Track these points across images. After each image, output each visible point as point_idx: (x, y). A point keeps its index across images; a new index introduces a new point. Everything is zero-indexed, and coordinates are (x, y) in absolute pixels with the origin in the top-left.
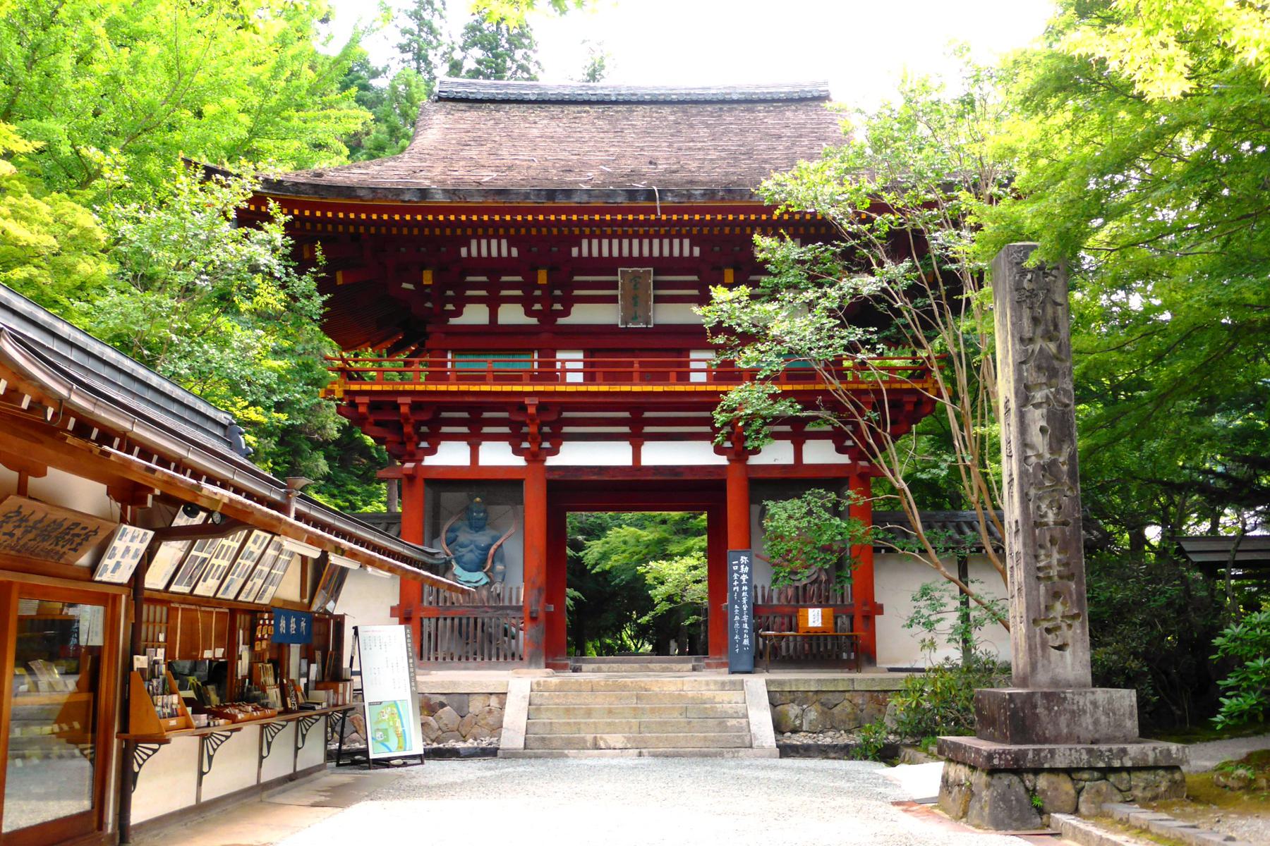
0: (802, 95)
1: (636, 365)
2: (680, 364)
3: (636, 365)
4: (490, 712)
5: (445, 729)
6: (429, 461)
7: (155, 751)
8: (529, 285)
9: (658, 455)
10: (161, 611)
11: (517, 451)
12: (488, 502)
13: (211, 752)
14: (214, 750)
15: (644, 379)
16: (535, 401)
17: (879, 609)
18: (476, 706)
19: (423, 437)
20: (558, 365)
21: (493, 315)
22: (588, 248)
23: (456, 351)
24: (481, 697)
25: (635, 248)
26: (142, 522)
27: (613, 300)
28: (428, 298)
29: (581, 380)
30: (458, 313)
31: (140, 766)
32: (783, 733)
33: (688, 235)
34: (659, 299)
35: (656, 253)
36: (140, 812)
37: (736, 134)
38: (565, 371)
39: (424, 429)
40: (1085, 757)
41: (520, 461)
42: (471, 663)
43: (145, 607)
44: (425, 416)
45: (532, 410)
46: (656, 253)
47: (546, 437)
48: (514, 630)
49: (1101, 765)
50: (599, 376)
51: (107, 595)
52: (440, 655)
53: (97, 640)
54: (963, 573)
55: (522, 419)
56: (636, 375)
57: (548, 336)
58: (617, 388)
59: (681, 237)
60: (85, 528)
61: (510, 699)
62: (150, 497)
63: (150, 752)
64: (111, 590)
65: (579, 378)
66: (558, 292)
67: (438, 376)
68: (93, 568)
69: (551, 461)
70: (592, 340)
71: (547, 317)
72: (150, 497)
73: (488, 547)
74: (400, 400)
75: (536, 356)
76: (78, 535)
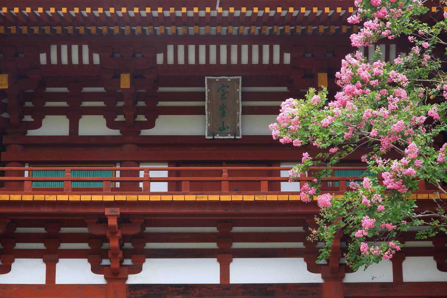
1: (225, 174)
3: (225, 174)
8: (112, 96)
9: (246, 272)
11: (96, 269)
15: (235, 188)
16: (117, 211)
20: (142, 174)
21: (74, 127)
22: (174, 55)
23: (31, 163)
27: (200, 111)
34: (247, 111)
41: (99, 279)
45: (113, 222)
46: (245, 60)
56: (225, 185)
57: (133, 148)
58: (204, 198)
65: (163, 187)
69: (133, 279)
70: (177, 153)
71: (131, 129)
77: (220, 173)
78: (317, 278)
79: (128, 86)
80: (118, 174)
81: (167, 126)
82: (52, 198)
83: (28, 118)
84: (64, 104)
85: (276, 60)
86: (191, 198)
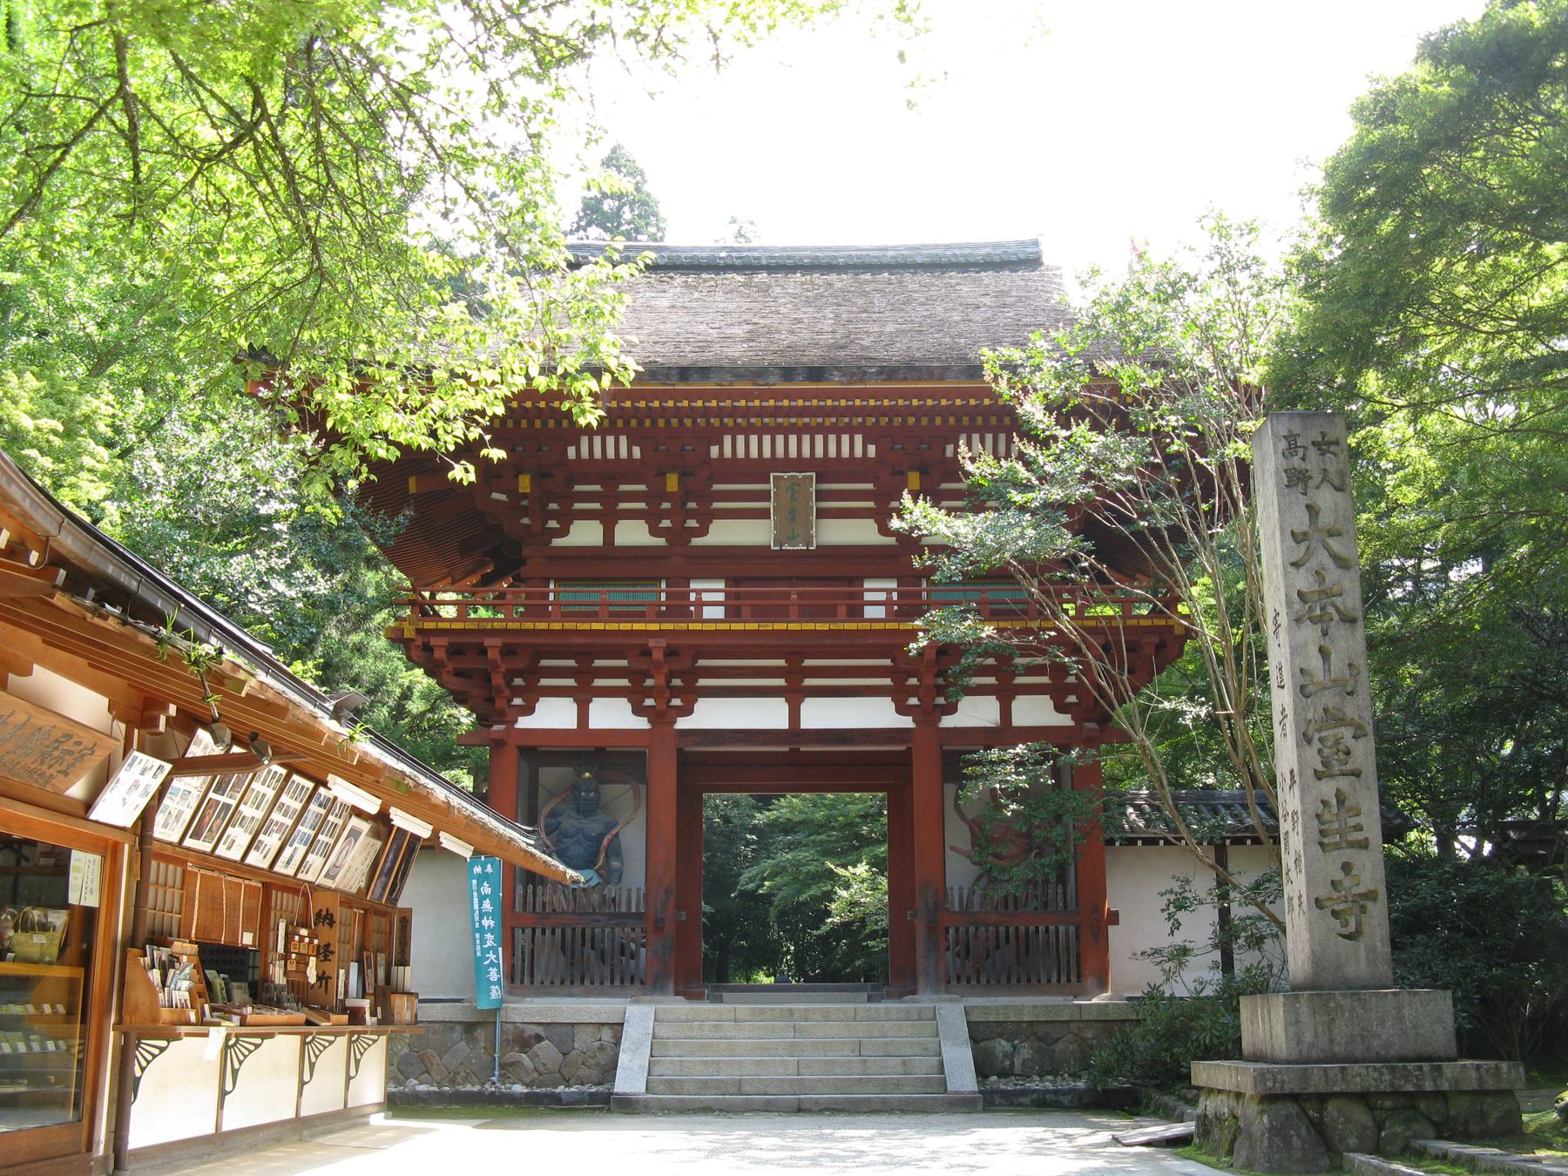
0: (1006, 258)
2: (851, 596)
4: (601, 1048)
5: (542, 1069)
6: (524, 723)
7: (162, 1050)
8: (655, 496)
9: (820, 714)
10: (174, 872)
11: (638, 710)
12: (601, 779)
13: (236, 1065)
14: (241, 1063)
15: (804, 615)
16: (663, 642)
17: (1114, 918)
18: (583, 1040)
19: (517, 691)
20: (693, 597)
21: (609, 534)
22: (732, 447)
23: (557, 580)
24: (590, 1029)
25: (793, 446)
26: (157, 750)
27: (764, 514)
28: (525, 512)
29: (722, 616)
30: (564, 532)
31: (143, 1069)
32: (987, 1077)
33: (861, 429)
34: (823, 514)
35: (819, 453)
36: (137, 1138)
37: (922, 304)
38: (701, 604)
39: (518, 681)
40: (1387, 1077)
41: (642, 723)
42: (577, 988)
43: (154, 863)
44: (519, 663)
45: (493, 655)
46: (819, 453)
47: (675, 692)
48: (633, 946)
49: (1410, 1088)
50: (745, 611)
51: (106, 841)
52: (538, 977)
53: (92, 901)
54: (1221, 859)
55: (645, 667)
56: (794, 610)
58: (769, 626)
59: (851, 431)
60: (79, 743)
61: (628, 1031)
62: (163, 719)
63: (156, 1051)
64: (115, 836)
65: (719, 613)
66: (692, 505)
67: (537, 610)
68: (89, 805)
69: (683, 723)
70: (734, 565)
71: (679, 536)
72: (163, 719)
73: (602, 836)
74: (488, 642)
75: (663, 586)
76: (70, 752)
77: (787, 595)
78: (907, 722)
79: (675, 489)
80: (663, 596)
81: (724, 533)
82: (586, 626)
83: (553, 524)
84: (597, 506)
85: (858, 453)
86: (753, 626)
